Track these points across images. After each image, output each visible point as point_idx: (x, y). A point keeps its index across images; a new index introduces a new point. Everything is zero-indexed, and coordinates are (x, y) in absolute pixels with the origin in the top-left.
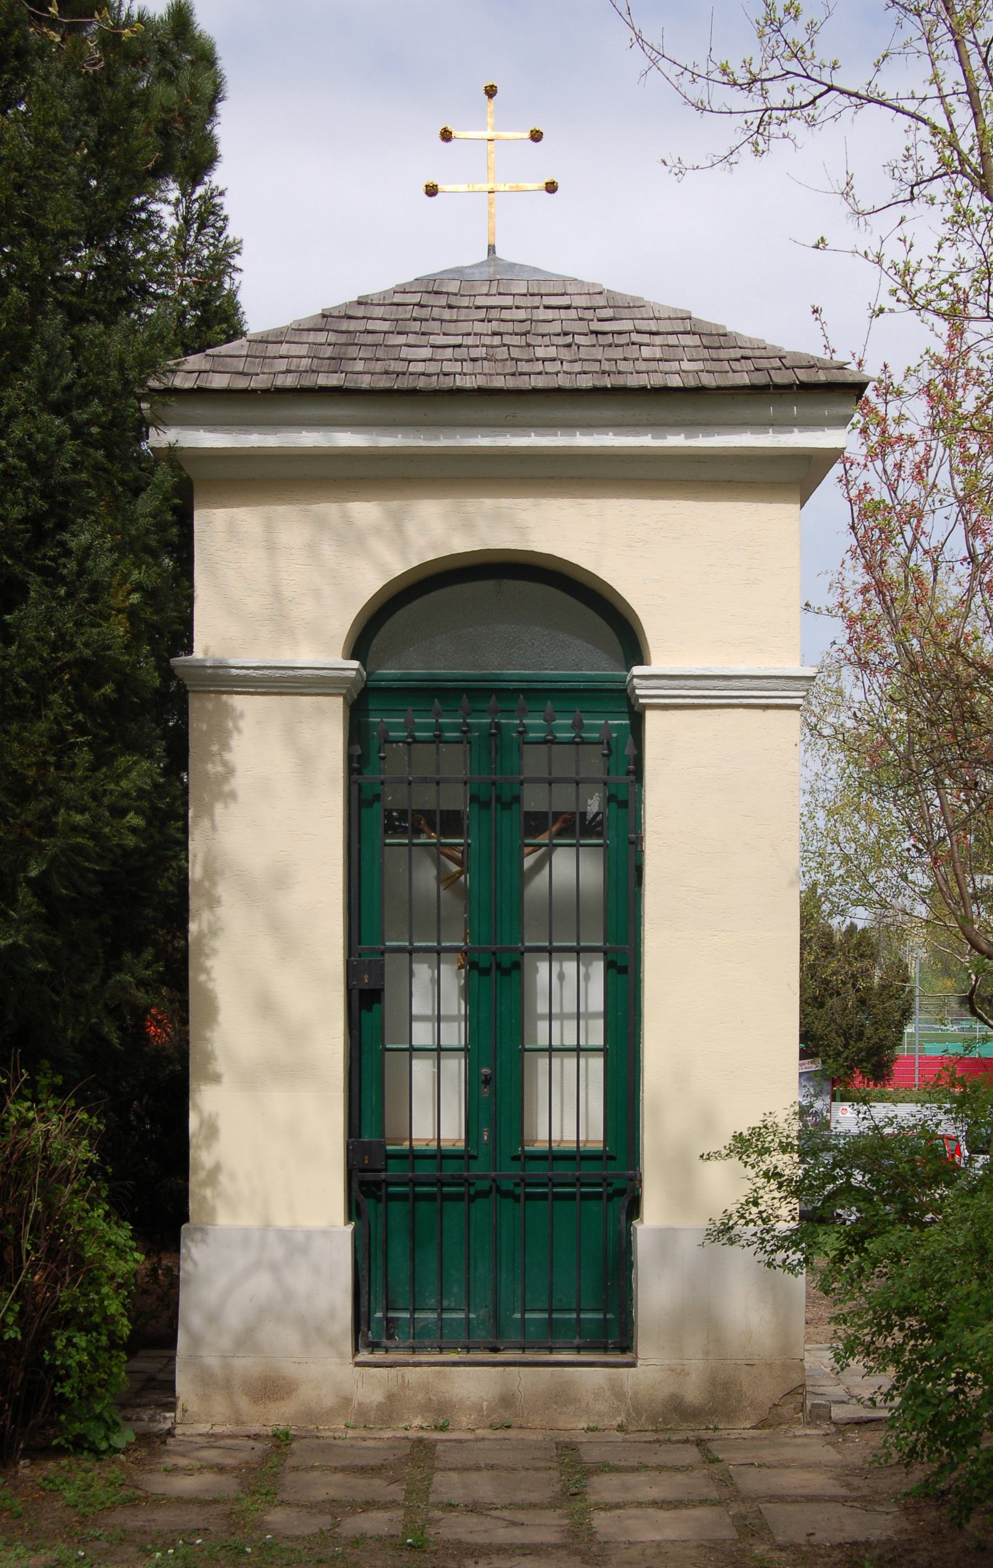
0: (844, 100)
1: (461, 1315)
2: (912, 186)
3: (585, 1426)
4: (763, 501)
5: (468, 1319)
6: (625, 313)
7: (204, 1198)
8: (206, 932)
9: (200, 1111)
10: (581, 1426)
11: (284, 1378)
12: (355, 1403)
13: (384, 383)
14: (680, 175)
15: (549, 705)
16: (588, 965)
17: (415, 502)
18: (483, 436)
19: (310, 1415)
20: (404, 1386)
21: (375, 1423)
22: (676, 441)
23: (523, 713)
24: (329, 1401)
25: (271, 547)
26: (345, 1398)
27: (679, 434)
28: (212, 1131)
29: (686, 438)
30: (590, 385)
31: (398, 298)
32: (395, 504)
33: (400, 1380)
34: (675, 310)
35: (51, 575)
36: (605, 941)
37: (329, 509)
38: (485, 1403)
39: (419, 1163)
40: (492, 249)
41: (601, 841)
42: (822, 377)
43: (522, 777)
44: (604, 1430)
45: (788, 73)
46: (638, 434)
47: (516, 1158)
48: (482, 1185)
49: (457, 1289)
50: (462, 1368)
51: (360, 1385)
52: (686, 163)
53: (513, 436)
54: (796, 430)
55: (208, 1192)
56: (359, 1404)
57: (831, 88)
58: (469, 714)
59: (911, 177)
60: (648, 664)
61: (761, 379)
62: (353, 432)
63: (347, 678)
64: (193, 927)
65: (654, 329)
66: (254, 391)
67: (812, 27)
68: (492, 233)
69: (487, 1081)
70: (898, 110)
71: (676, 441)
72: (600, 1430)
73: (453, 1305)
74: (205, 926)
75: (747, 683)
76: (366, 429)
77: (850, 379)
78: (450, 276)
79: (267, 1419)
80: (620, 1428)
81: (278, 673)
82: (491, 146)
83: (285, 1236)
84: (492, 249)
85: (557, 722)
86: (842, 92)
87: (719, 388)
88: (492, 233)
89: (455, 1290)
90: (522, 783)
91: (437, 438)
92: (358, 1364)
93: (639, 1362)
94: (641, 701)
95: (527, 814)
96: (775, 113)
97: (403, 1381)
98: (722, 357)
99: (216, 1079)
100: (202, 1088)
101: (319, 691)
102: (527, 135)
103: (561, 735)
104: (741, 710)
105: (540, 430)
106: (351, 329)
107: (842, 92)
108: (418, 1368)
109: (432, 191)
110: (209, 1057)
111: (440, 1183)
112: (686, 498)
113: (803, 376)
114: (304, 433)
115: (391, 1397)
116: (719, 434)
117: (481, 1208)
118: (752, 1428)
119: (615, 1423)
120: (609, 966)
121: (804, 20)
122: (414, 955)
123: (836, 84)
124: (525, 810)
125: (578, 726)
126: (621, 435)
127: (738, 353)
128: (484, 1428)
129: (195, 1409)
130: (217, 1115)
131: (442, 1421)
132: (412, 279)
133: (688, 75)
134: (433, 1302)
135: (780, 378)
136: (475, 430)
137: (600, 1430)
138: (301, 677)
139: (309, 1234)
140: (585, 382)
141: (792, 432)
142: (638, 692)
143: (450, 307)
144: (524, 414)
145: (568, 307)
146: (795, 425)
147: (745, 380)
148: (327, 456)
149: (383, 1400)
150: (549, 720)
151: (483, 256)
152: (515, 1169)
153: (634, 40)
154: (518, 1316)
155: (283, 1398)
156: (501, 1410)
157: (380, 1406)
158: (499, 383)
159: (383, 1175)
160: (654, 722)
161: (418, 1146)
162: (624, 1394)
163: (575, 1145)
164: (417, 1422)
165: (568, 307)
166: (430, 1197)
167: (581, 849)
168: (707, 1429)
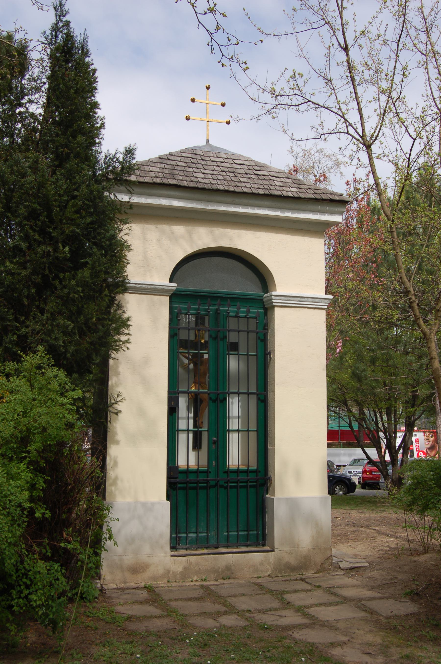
0: (313, 106)
1: (205, 534)
2: (321, 135)
3: (257, 576)
4: (312, 237)
5: (207, 536)
6: (263, 169)
7: (111, 490)
8: (114, 384)
9: (110, 456)
10: (255, 576)
11: (144, 563)
12: (171, 572)
13: (192, 185)
14: (237, 121)
15: (238, 304)
16: (232, 399)
17: (196, 228)
18: (224, 207)
19: (155, 578)
20: (190, 564)
21: (179, 580)
22: (288, 214)
23: (229, 306)
24: (161, 571)
25: (144, 239)
26: (168, 570)
27: (289, 212)
28: (116, 464)
29: (292, 214)
30: (263, 193)
31: (183, 155)
32: (190, 228)
33: (189, 562)
34: (279, 170)
35: (99, 245)
36: (257, 390)
37: (166, 227)
38: (220, 569)
39: (190, 475)
40: (208, 141)
41: (186, 351)
42: (337, 198)
43: (179, 327)
44: (264, 577)
45: (296, 94)
46: (276, 211)
47: (225, 472)
48: (212, 483)
49: (203, 524)
50: (211, 556)
51: (173, 564)
52: (240, 118)
53: (234, 207)
54: (326, 214)
55: (113, 488)
56: (173, 572)
57: (309, 101)
58: (210, 305)
59: (320, 131)
60: (276, 291)
61: (317, 197)
62: (178, 201)
63: (172, 290)
64: (110, 383)
65: (276, 176)
66: (146, 183)
67: (306, 81)
68: (208, 135)
69: (214, 443)
70: (332, 111)
71: (288, 214)
72: (262, 577)
73: (201, 530)
74: (114, 382)
75: (310, 300)
76: (183, 200)
77: (343, 199)
78: (198, 149)
79: (137, 581)
80: (269, 576)
81: (147, 286)
82: (208, 106)
83: (144, 505)
84: (208, 141)
85: (241, 310)
86: (313, 103)
87: (305, 198)
88: (208, 135)
89: (202, 524)
90: (179, 329)
91: (208, 206)
92: (172, 556)
93: (275, 550)
94: (274, 304)
95: (181, 340)
96: (283, 106)
97: (190, 562)
98: (302, 187)
99: (117, 442)
100: (112, 446)
101: (161, 294)
102: (220, 104)
103: (241, 315)
104: (307, 309)
105: (252, 207)
106: (172, 164)
107: (313, 103)
108: (195, 557)
109: (188, 118)
110: (115, 434)
111: (186, 483)
112: (288, 234)
113: (332, 197)
114: (161, 200)
115: (185, 568)
116: (302, 213)
117: (212, 492)
118: (315, 573)
119: (267, 574)
120: (259, 399)
121: (304, 78)
122: (250, 395)
123: (311, 100)
124: (181, 338)
125: (248, 311)
126: (270, 211)
127: (308, 187)
128: (220, 579)
129: (108, 578)
130: (117, 457)
131: (204, 578)
132: (184, 148)
133: (261, 90)
134: (194, 530)
135: (324, 197)
136: (221, 204)
137: (262, 577)
138: (155, 288)
139: (153, 504)
140: (261, 192)
141: (325, 215)
142: (273, 301)
143: (203, 160)
144: (238, 200)
145: (243, 165)
146: (326, 213)
147: (312, 196)
148: (213, 213)
149: (182, 570)
150: (239, 309)
151: (205, 143)
152: (224, 476)
153: (232, 75)
154: (226, 534)
155: (143, 572)
156: (226, 572)
157: (181, 573)
158: (232, 189)
159: (178, 480)
160: (278, 312)
161: (231, 467)
162: (270, 563)
163: (187, 467)
164: (195, 578)
165: (243, 165)
166: (234, 487)
167: (230, 356)
168: (299, 574)
